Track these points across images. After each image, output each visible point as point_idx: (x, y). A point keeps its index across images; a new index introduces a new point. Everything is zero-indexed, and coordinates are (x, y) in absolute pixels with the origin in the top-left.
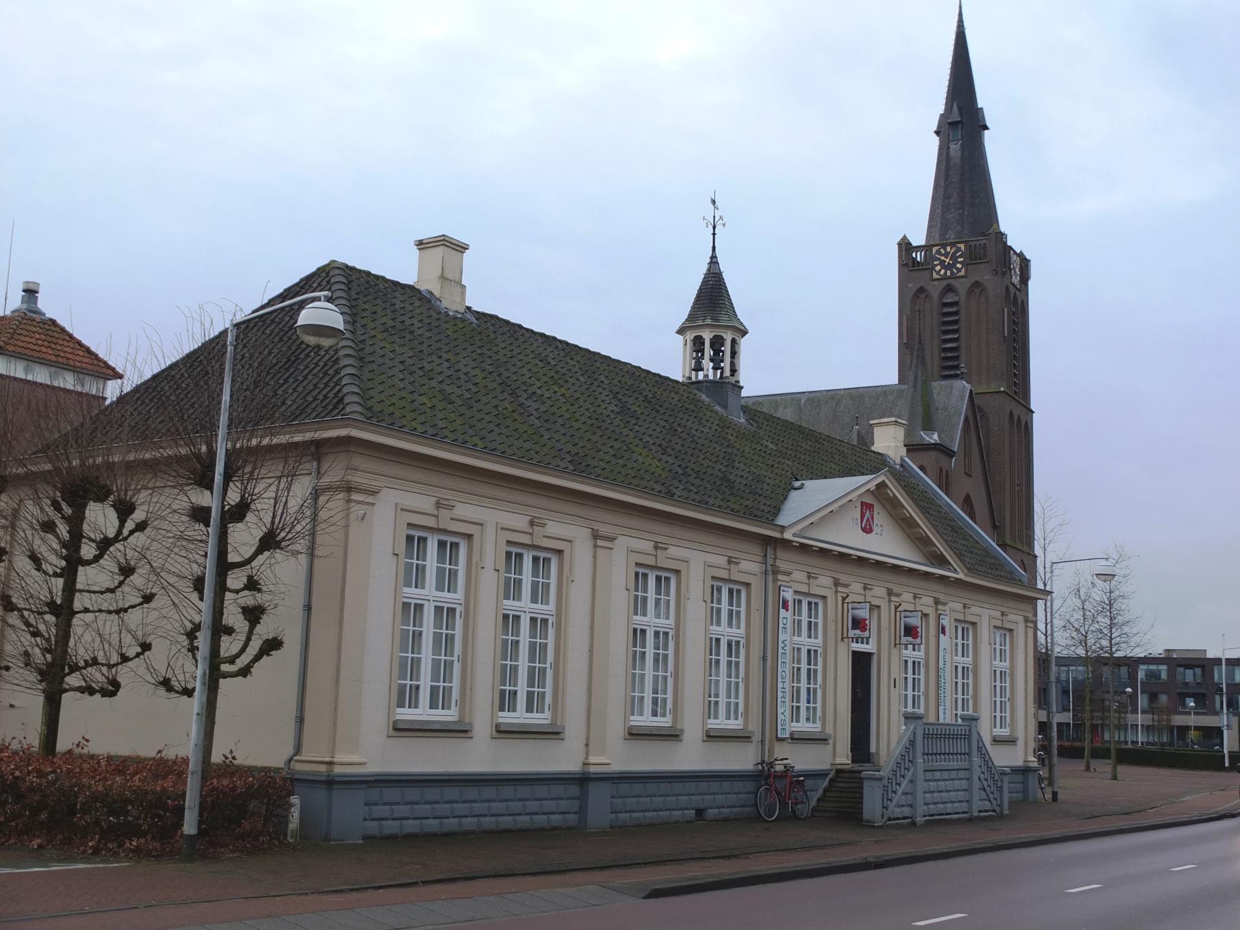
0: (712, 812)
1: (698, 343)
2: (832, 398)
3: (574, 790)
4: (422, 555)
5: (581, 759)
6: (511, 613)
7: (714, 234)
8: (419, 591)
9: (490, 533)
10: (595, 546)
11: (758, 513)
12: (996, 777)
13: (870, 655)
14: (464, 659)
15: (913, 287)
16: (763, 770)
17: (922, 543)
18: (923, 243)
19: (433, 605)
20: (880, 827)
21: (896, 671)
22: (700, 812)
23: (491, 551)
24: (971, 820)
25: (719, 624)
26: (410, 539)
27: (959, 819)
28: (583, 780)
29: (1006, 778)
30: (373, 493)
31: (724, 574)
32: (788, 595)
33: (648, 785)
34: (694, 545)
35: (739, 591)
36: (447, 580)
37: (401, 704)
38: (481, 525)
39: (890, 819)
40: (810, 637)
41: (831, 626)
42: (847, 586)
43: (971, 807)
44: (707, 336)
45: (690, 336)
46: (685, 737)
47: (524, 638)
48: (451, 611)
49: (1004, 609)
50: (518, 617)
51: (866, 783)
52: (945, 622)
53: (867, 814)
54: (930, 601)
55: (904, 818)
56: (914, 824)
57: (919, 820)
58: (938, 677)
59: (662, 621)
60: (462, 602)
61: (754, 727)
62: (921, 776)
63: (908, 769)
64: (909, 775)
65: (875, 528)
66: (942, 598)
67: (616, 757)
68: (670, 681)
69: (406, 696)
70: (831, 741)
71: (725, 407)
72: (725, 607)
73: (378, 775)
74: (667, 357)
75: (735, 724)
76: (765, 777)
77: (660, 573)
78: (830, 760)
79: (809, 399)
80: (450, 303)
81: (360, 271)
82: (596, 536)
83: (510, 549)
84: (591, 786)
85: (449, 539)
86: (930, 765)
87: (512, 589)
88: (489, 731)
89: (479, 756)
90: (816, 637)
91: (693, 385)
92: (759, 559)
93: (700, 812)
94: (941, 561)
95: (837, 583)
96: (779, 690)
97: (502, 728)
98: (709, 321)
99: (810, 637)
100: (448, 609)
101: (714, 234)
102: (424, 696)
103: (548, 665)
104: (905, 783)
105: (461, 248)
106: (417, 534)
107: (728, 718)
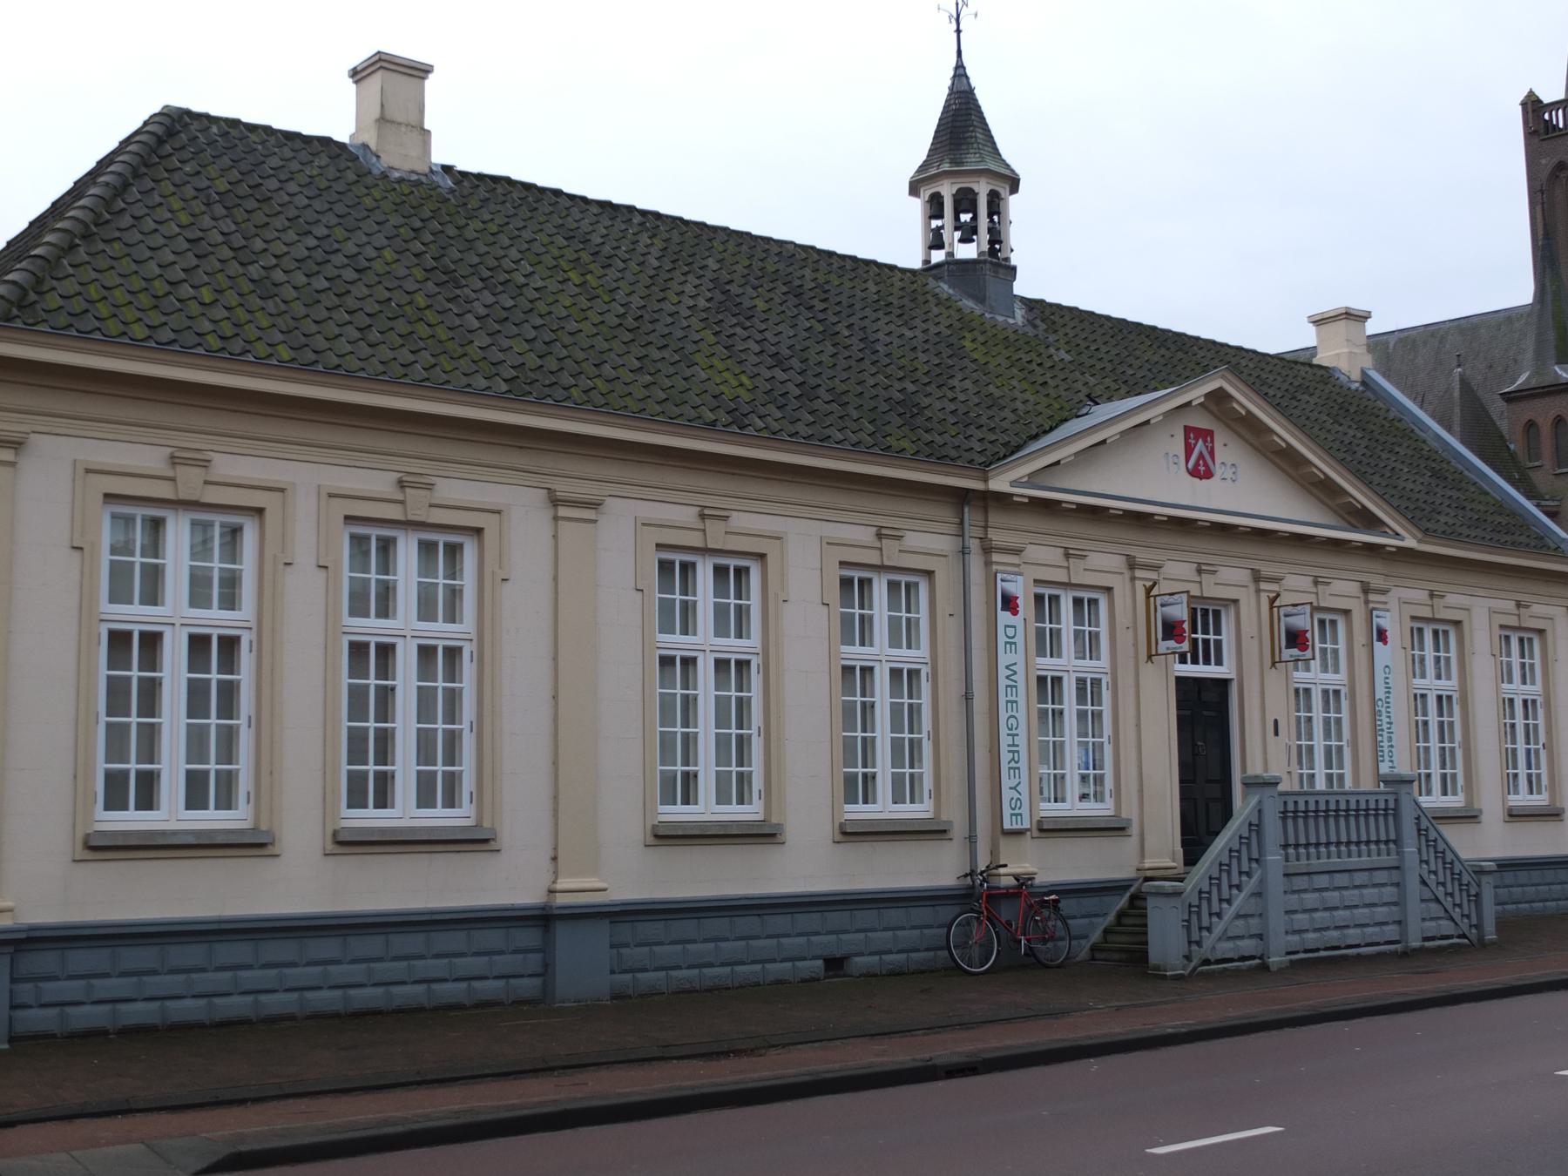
0: (860, 963)
1: (935, 207)
2: (1433, 335)
3: (529, 937)
4: (1055, 617)
5: (545, 881)
6: (1050, 674)
7: (958, 31)
8: (1055, 661)
9: (305, 507)
10: (556, 518)
11: (954, 454)
12: (1466, 879)
13: (1223, 684)
14: (257, 722)
15: (1547, 163)
16: (973, 887)
17: (1324, 490)
18: (1562, 96)
19: (887, 667)
20: (1180, 978)
21: (1280, 706)
22: (835, 964)
23: (1481, 636)
24: (1407, 954)
25: (1423, 676)
26: (846, 583)
27: (1379, 955)
28: (544, 919)
29: (1487, 881)
30: (595, 505)
31: (1426, 613)
32: (1019, 587)
33: (858, 914)
34: (790, 510)
35: (1446, 633)
36: (733, 621)
37: (851, 798)
38: (282, 490)
39: (1207, 962)
40: (1524, 683)
41: (1125, 639)
42: (1155, 568)
43: (1404, 933)
44: (947, 190)
45: (926, 193)
46: (1484, 818)
47: (1318, 714)
48: (914, 674)
49: (1519, 597)
50: (1060, 679)
51: (1151, 903)
52: (1386, 621)
53: (1154, 956)
54: (1354, 588)
55: (1243, 959)
56: (1264, 967)
57: (1275, 960)
58: (1375, 714)
59: (1330, 676)
60: (473, 636)
61: (954, 815)
62: (1276, 883)
63: (1249, 874)
64: (1250, 885)
65: (1218, 471)
66: (1376, 581)
67: (625, 874)
68: (1459, 754)
69: (859, 787)
70: (1134, 830)
71: (981, 300)
72: (1516, 660)
73: (433, 912)
74: (893, 234)
75: (918, 811)
76: (979, 897)
77: (1080, 594)
78: (1135, 863)
79: (1400, 340)
80: (396, 158)
81: (543, 190)
82: (555, 502)
83: (848, 573)
84: (562, 931)
85: (732, 563)
86: (1294, 865)
87: (1047, 643)
88: (641, 837)
89: (297, 884)
90: (1533, 683)
91: (929, 268)
92: (952, 529)
93: (835, 964)
94: (1368, 521)
95: (1257, 577)
96: (1004, 749)
97: (341, 838)
98: (946, 167)
99: (1439, 677)
100: (1053, 678)
101: (958, 31)
102: (884, 787)
103: (1105, 739)
104: (1240, 899)
105: (421, 71)
106: (1047, 591)
107: (1445, 793)
